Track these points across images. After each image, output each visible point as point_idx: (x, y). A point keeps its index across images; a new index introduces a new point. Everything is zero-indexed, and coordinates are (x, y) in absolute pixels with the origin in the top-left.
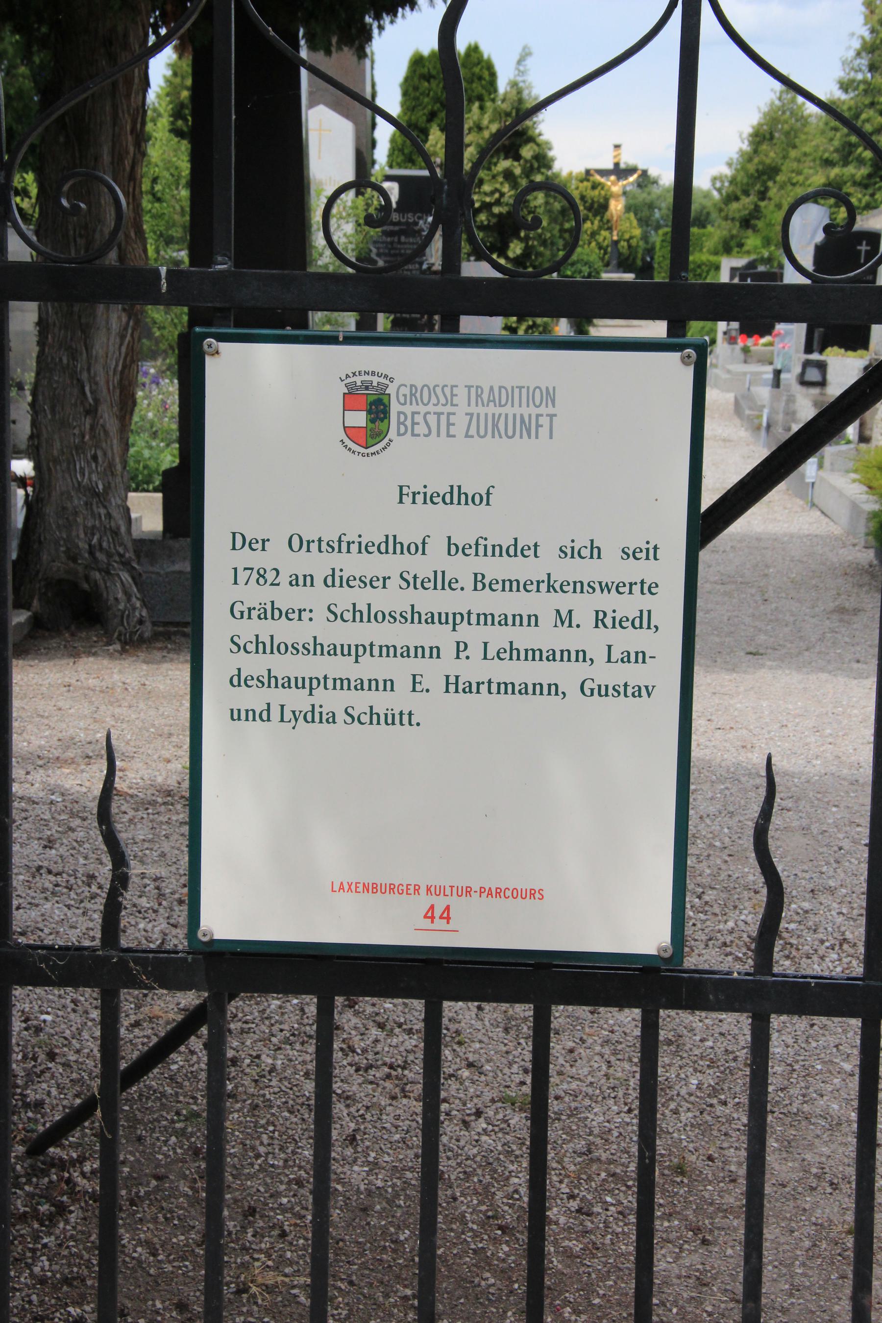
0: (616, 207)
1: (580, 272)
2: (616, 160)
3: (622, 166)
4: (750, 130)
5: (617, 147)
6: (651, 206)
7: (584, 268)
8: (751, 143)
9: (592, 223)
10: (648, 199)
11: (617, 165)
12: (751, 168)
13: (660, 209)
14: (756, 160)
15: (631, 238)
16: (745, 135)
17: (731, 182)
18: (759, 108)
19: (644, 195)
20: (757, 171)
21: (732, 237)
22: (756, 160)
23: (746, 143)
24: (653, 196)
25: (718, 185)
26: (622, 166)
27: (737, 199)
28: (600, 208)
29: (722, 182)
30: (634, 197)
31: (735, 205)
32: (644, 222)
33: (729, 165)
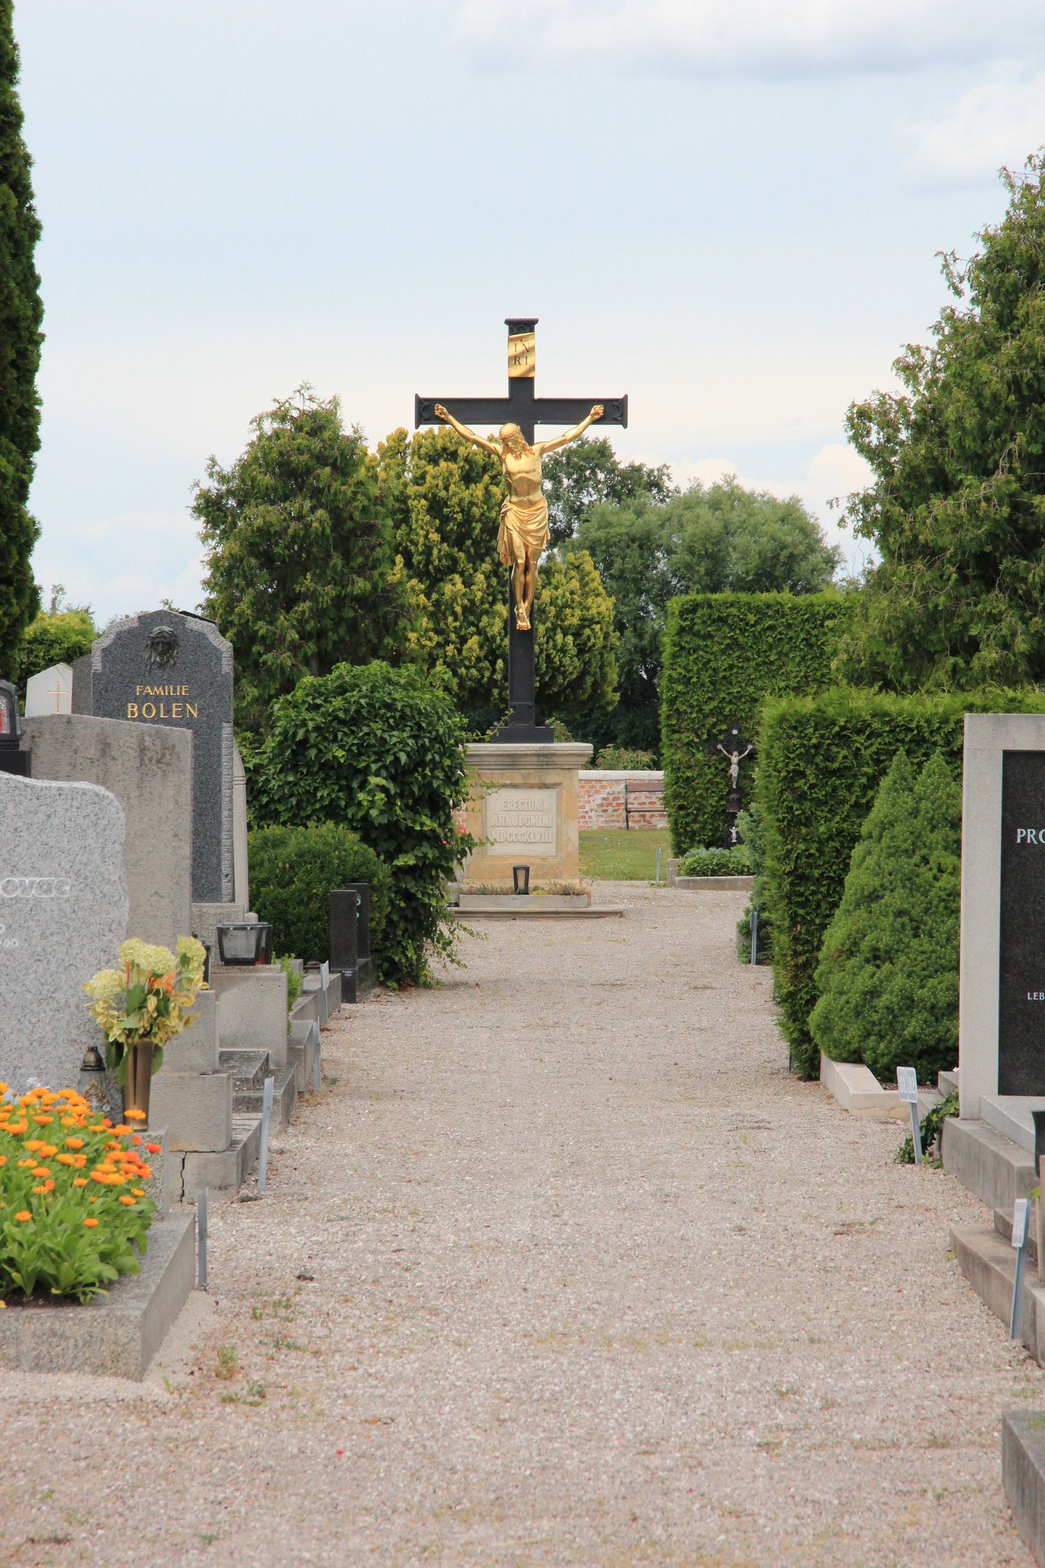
0: (524, 525)
1: (382, 749)
2: (517, 371)
3: (542, 391)
4: (982, 250)
5: (521, 327)
6: (645, 543)
7: (394, 737)
8: (986, 293)
9: (468, 583)
10: (639, 526)
11: (521, 384)
12: (992, 374)
13: (669, 552)
14: (1009, 349)
15: (587, 622)
16: (961, 268)
17: (918, 429)
18: (1006, 174)
19: (629, 516)
20: (1014, 385)
21: (933, 618)
22: (1009, 349)
23: (969, 293)
24: (651, 518)
25: (875, 437)
26: (542, 391)
27: (946, 485)
28: (474, 536)
29: (889, 425)
30: (605, 524)
31: (940, 506)
32: (628, 582)
33: (909, 371)
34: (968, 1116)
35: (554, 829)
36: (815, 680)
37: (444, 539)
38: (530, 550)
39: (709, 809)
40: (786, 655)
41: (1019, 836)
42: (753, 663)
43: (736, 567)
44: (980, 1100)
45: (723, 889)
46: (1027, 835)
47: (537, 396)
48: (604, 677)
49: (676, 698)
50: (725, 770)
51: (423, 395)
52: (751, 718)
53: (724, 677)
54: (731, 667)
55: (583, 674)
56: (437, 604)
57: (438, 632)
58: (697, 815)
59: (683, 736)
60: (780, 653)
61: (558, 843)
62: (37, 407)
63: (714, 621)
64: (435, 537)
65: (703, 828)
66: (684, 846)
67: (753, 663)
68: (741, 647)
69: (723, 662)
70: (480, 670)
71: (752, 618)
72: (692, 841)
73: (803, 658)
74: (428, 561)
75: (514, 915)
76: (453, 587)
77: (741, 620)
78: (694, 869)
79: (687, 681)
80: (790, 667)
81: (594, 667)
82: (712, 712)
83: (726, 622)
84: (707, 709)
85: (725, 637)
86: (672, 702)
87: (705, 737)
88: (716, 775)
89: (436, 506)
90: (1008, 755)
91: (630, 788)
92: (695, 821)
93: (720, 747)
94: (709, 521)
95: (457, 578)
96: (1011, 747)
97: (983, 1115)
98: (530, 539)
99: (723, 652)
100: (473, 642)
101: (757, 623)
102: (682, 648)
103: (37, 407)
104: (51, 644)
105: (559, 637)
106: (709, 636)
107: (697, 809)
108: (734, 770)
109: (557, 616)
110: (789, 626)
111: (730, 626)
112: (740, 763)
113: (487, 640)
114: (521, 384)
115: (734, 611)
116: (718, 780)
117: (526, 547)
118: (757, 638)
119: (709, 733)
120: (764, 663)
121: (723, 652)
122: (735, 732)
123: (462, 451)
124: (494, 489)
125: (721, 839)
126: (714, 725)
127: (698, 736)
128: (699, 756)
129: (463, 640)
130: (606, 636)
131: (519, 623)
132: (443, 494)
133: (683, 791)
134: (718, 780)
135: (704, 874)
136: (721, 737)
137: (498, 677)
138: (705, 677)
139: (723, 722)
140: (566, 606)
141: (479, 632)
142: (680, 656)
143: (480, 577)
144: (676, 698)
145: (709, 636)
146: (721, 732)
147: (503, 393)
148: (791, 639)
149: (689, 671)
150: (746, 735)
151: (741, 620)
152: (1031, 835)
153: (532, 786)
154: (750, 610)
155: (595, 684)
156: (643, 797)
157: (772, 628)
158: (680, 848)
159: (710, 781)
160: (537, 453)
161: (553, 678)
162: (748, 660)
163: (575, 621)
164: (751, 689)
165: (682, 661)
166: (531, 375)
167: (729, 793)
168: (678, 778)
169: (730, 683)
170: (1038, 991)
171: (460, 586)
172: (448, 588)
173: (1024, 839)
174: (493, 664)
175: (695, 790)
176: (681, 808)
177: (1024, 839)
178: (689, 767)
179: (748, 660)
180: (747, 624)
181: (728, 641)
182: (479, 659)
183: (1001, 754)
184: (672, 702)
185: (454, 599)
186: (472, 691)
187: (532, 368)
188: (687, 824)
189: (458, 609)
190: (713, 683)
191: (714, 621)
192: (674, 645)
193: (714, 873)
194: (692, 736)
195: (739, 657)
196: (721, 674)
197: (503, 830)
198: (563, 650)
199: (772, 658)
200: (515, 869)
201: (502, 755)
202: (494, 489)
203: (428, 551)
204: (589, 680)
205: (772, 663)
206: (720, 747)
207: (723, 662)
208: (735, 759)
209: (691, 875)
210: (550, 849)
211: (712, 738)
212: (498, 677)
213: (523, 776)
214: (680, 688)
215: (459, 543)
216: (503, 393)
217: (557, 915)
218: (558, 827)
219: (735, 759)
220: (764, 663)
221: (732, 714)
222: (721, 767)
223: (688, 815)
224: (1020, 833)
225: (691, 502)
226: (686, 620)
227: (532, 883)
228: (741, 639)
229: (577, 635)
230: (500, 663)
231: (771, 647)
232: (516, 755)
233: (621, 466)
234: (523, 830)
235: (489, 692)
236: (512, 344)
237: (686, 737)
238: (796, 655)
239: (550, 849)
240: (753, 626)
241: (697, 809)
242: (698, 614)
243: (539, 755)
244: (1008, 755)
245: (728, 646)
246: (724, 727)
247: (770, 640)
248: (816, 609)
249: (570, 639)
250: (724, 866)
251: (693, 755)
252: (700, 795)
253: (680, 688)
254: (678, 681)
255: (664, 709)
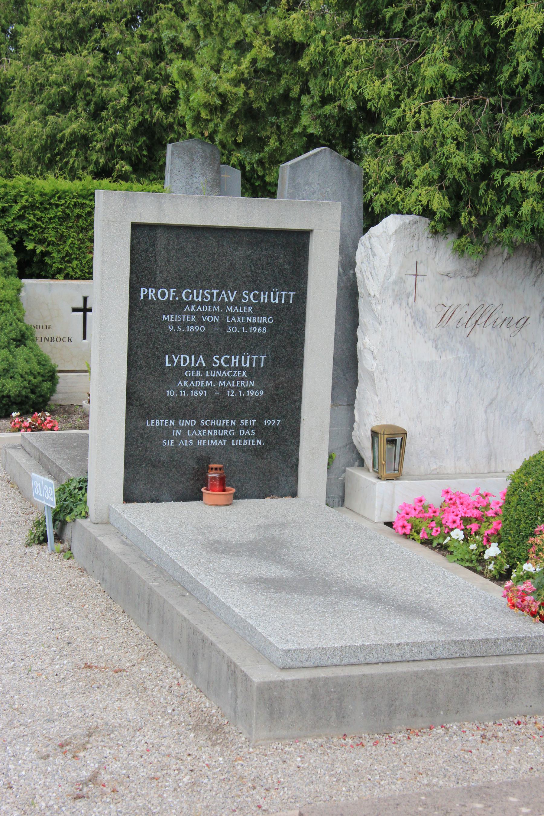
3: (89, 314)
26: (89, 314)
34: (99, 521)
41: (142, 294)
44: (109, 509)
46: (148, 293)
62: (239, 51)
90: (135, 226)
96: (138, 220)
97: (112, 521)
103: (239, 51)
152: (151, 293)
170: (155, 419)
173: (146, 296)
177: (146, 296)
183: (129, 226)
224: (143, 292)
233: (447, 205)
244: (135, 226)
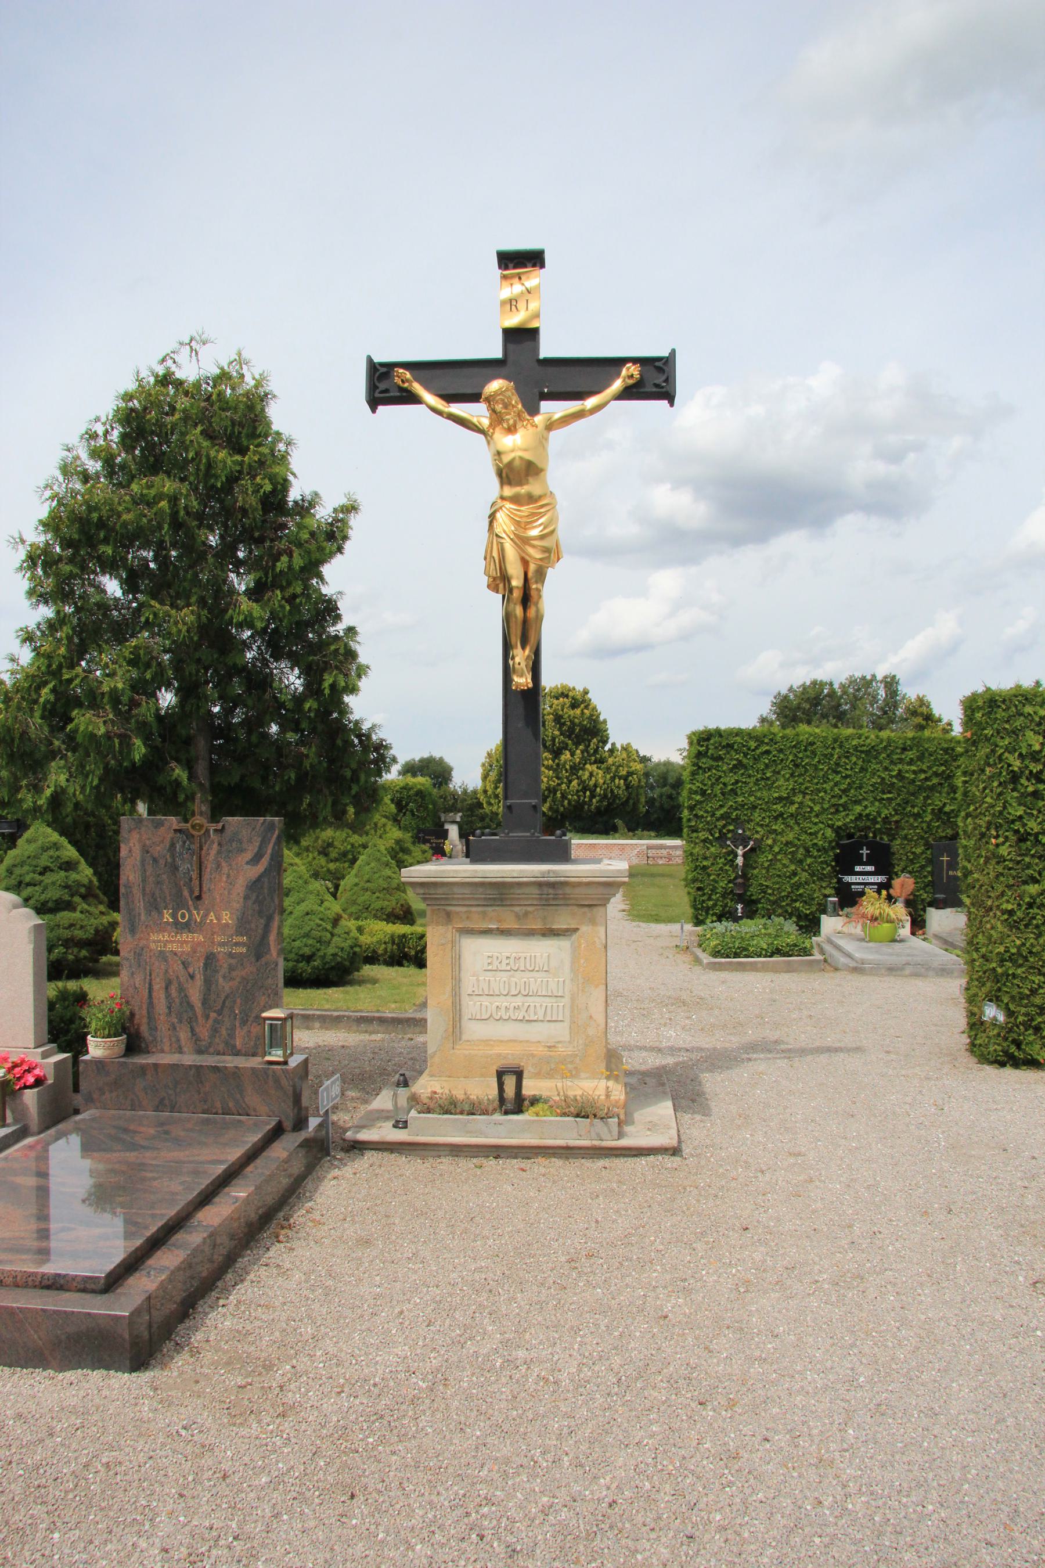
2: (513, 321)
3: (549, 348)
5: (519, 261)
9: (573, 754)
11: (521, 337)
24: (649, 768)
35: (567, 1000)
36: (800, 791)
37: (561, 734)
38: (532, 567)
39: (720, 890)
40: (779, 773)
42: (753, 779)
43: (671, 781)
45: (744, 970)
47: (542, 356)
48: (638, 800)
49: (695, 805)
50: (732, 861)
51: (377, 359)
52: (752, 821)
53: (732, 790)
54: (737, 782)
55: (628, 799)
56: (558, 765)
57: (558, 778)
58: (711, 895)
59: (700, 834)
60: (774, 772)
61: (572, 1022)
63: (724, 747)
64: (557, 733)
65: (715, 905)
66: (701, 918)
67: (753, 779)
68: (745, 767)
69: (730, 779)
70: (579, 797)
71: (753, 744)
72: (707, 913)
73: (792, 775)
74: (554, 744)
75: (497, 1152)
76: (566, 756)
77: (744, 746)
78: (719, 952)
79: (703, 793)
80: (781, 782)
81: (634, 795)
82: (722, 817)
83: (732, 747)
84: (718, 814)
85: (731, 760)
86: (691, 808)
87: (717, 835)
88: (725, 865)
89: (558, 719)
91: (649, 848)
92: (710, 899)
93: (728, 843)
94: (663, 769)
95: (567, 752)
98: (531, 551)
99: (731, 770)
100: (575, 783)
101: (756, 748)
102: (700, 768)
104: (410, 789)
105: (617, 781)
106: (720, 758)
107: (712, 890)
108: (740, 861)
109: (616, 771)
110: (781, 751)
111: (736, 750)
112: (744, 855)
113: (582, 782)
114: (521, 337)
115: (738, 739)
116: (727, 867)
117: (525, 563)
118: (756, 759)
119: (720, 832)
120: (762, 779)
121: (731, 770)
122: (740, 831)
123: (571, 694)
124: (586, 711)
125: (729, 912)
126: (724, 826)
127: (712, 835)
128: (713, 849)
129: (570, 782)
130: (640, 781)
131: (516, 679)
132: (561, 713)
133: (700, 877)
134: (727, 867)
135: (728, 957)
136: (729, 835)
137: (587, 799)
138: (717, 789)
139: (730, 824)
140: (620, 766)
141: (578, 778)
142: (698, 774)
143: (578, 752)
144: (695, 805)
145: (720, 758)
146: (729, 831)
147: (495, 350)
148: (782, 760)
149: (705, 785)
150: (748, 833)
151: (744, 746)
153: (530, 933)
154: (751, 738)
155: (634, 803)
156: (654, 851)
157: (768, 752)
158: (697, 918)
159: (721, 869)
160: (541, 426)
161: (614, 800)
162: (750, 776)
163: (624, 773)
164: (752, 799)
165: (700, 777)
166: (534, 325)
167: (736, 878)
168: (696, 867)
169: (736, 794)
171: (569, 756)
172: (563, 757)
174: (585, 793)
175: (709, 875)
176: (699, 889)
178: (706, 858)
179: (750, 776)
180: (749, 749)
181: (735, 762)
182: (578, 791)
184: (691, 808)
185: (565, 763)
186: (575, 806)
187: (537, 316)
188: (703, 901)
189: (568, 767)
190: (723, 794)
191: (724, 747)
192: (693, 765)
193: (736, 955)
194: (707, 835)
195: (743, 774)
196: (729, 788)
197: (486, 1001)
198: (618, 787)
199: (768, 775)
200: (500, 1075)
201: (482, 884)
202: (586, 711)
203: (553, 739)
204: (631, 802)
205: (768, 779)
206: (728, 843)
207: (730, 779)
208: (740, 852)
209: (716, 957)
210: (560, 1032)
211: (722, 838)
212: (587, 799)
213: (518, 917)
214: (698, 797)
215: (569, 737)
216: (495, 350)
217: (567, 1152)
218: (573, 999)
219: (740, 852)
220: (762, 779)
221: (738, 818)
222: (730, 858)
223: (704, 894)
225: (658, 764)
226: (702, 746)
227: (530, 1088)
228: (745, 761)
229: (625, 780)
230: (588, 793)
231: (767, 766)
232: (503, 885)
234: (518, 1001)
235: (583, 807)
236: (505, 283)
237: (703, 835)
238: (786, 773)
239: (560, 1032)
240: (753, 750)
241: (712, 890)
242: (712, 741)
243: (540, 885)
245: (735, 766)
246: (731, 828)
247: (767, 761)
248: (801, 738)
249: (622, 781)
250: (745, 949)
251: (708, 849)
252: (714, 880)
253: (698, 797)
254: (696, 793)
255: (686, 813)
